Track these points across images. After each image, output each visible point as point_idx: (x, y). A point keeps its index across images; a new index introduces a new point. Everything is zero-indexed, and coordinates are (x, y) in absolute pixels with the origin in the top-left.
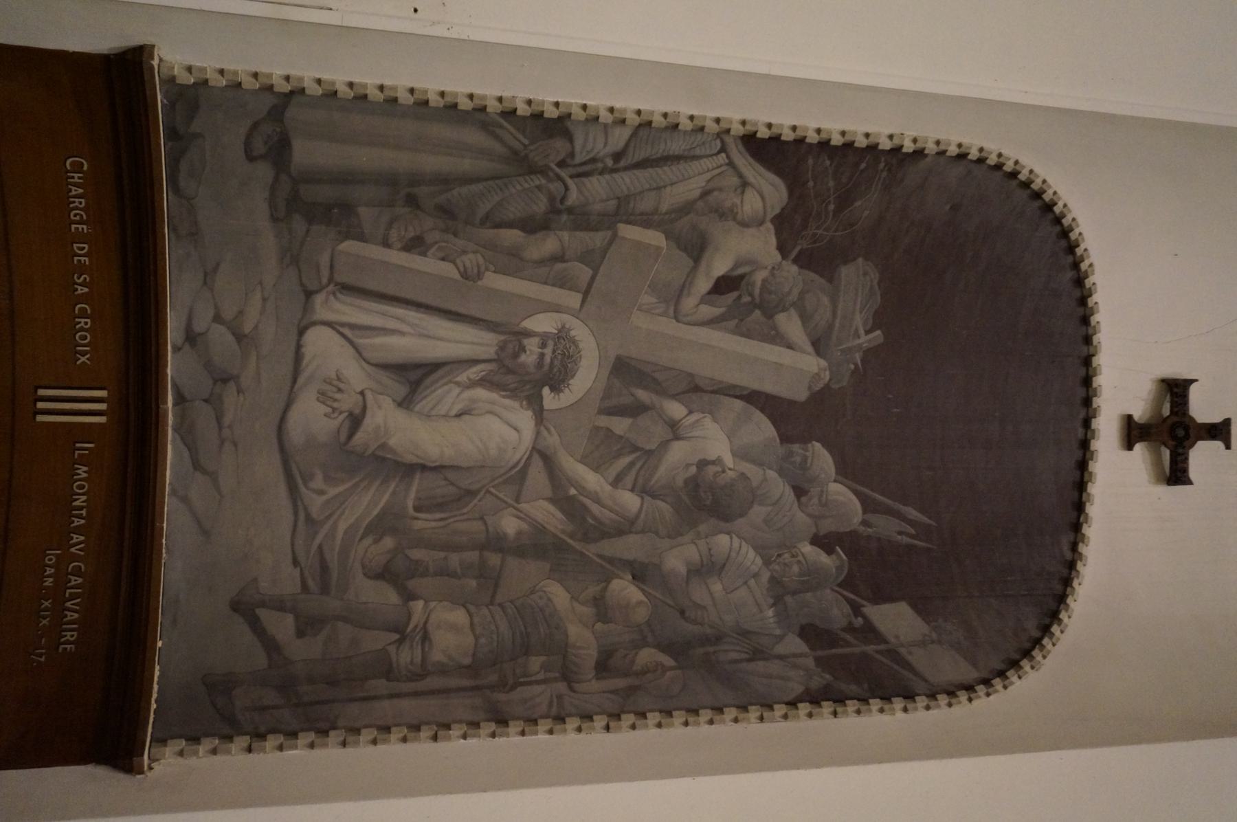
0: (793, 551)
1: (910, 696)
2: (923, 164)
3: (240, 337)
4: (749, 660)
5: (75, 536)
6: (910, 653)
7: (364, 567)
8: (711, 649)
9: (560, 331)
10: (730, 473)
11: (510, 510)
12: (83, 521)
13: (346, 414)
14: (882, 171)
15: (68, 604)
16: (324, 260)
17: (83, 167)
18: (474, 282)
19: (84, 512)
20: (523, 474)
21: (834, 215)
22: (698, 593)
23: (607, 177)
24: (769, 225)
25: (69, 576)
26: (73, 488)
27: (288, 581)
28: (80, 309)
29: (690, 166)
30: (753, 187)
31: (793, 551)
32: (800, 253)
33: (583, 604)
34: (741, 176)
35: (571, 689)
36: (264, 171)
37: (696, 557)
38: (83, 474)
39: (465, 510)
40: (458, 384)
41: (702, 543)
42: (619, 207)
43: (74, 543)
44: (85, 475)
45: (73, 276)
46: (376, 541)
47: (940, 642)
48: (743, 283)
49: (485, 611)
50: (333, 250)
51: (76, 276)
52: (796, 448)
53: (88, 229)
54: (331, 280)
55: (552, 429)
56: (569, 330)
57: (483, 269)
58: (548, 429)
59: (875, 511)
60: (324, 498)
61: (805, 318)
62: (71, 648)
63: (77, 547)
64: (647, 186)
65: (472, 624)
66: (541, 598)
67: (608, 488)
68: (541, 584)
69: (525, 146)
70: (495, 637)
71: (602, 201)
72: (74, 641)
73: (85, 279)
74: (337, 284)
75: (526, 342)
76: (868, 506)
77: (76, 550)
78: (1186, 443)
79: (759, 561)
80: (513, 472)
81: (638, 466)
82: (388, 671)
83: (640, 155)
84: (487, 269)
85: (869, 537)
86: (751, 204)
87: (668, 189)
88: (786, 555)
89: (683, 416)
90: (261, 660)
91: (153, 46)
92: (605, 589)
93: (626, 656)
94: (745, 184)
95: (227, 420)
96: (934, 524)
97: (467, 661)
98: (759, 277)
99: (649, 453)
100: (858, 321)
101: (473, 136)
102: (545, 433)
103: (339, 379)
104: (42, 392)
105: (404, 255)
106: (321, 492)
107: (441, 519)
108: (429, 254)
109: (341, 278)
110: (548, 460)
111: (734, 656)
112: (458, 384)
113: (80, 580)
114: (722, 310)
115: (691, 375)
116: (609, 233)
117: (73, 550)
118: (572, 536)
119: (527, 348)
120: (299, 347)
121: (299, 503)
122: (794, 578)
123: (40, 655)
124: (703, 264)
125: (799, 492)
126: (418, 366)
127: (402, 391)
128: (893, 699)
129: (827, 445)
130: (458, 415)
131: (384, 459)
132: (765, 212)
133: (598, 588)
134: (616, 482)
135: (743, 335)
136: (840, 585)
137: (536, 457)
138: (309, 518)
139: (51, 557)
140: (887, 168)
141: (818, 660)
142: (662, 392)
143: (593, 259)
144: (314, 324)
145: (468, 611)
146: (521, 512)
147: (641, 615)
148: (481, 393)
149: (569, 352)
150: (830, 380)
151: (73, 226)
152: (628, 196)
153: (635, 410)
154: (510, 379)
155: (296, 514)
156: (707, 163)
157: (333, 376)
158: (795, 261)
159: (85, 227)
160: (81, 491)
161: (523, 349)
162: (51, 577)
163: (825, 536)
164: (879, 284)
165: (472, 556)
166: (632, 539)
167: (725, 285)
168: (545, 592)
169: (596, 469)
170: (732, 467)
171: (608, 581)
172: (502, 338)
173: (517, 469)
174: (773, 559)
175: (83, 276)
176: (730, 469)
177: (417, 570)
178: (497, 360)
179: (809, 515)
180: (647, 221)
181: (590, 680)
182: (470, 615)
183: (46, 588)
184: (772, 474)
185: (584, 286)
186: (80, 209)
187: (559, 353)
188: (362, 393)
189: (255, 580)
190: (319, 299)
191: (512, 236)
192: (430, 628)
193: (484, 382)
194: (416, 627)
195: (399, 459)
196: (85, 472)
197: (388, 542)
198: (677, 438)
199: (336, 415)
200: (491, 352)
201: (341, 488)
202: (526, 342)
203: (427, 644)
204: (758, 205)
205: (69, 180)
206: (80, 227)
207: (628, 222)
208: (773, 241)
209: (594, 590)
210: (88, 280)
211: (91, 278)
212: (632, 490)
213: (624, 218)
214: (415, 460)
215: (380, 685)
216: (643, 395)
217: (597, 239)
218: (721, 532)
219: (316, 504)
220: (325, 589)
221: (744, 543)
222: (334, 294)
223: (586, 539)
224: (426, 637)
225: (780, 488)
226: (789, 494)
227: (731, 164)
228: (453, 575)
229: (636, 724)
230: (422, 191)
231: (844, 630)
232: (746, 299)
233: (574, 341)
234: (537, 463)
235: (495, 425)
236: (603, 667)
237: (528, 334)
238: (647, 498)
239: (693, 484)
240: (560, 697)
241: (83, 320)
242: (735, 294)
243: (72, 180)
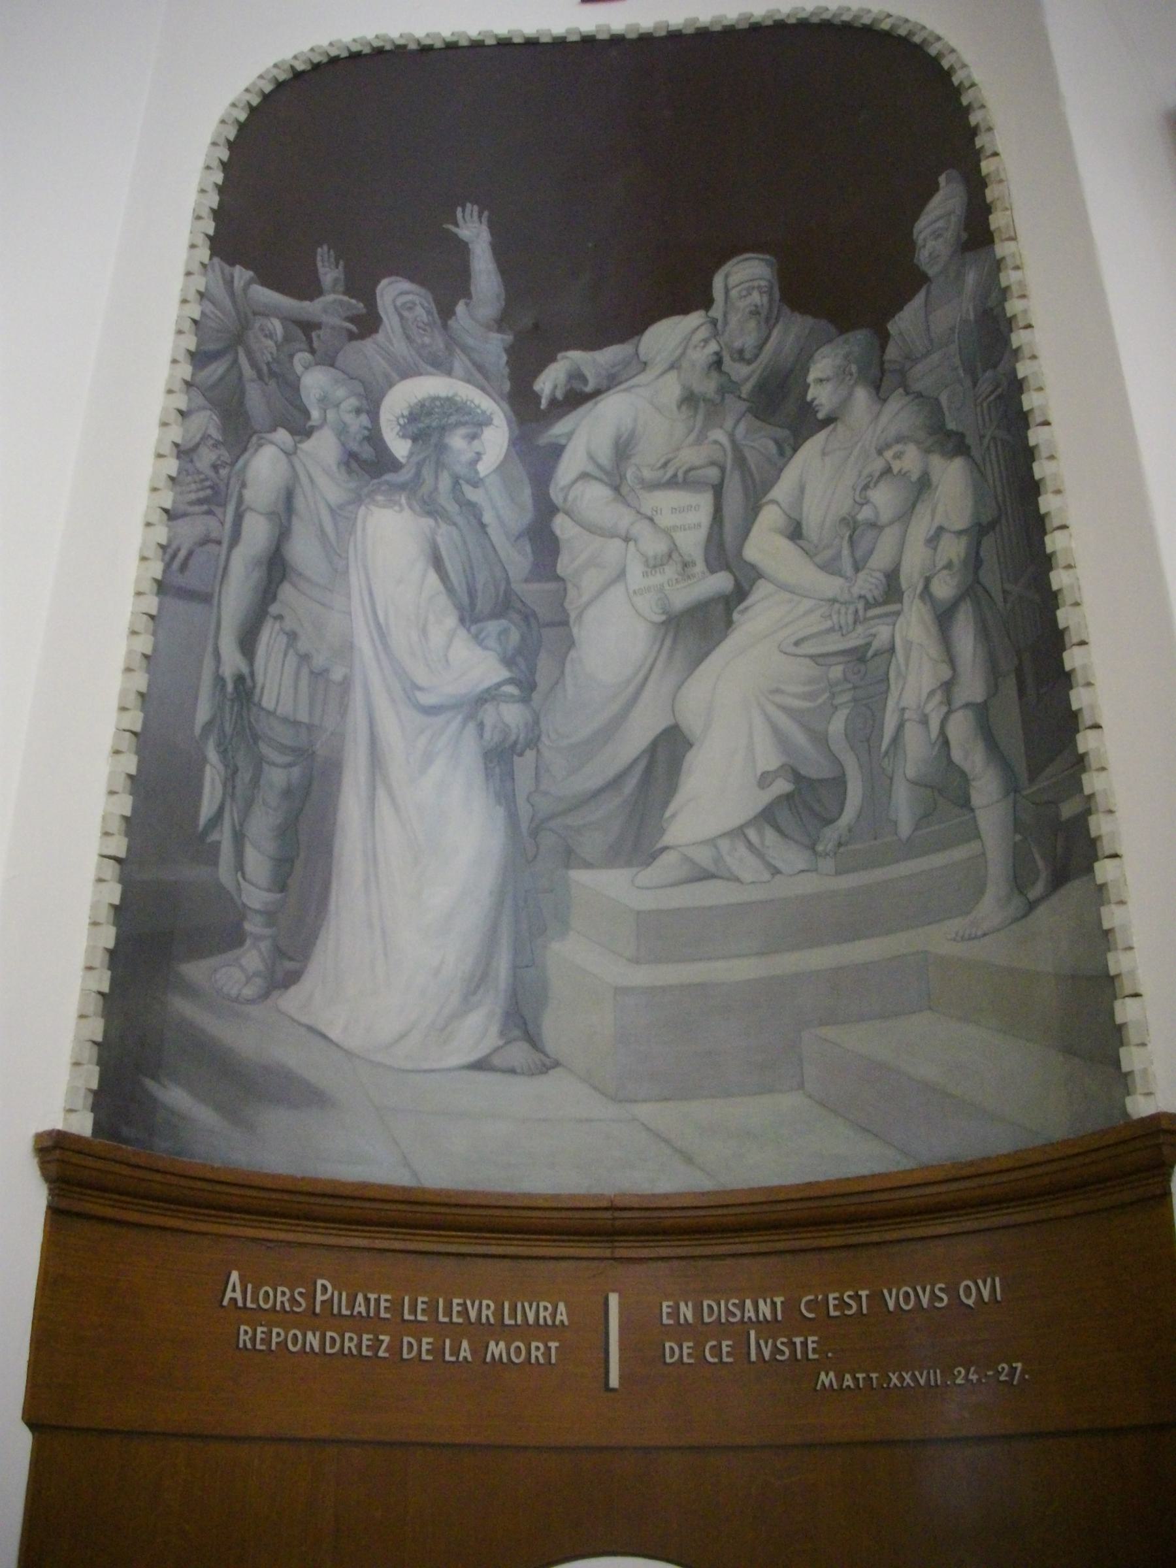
5: (229, 1294)
17: (812, 1300)
44: (502, 1345)
62: (668, 1307)
72: (357, 1335)
73: (782, 1343)
128: (1009, 315)
151: (425, 1357)
160: (715, 1308)
162: (757, 1302)
175: (847, 1300)
196: (497, 1345)
241: (242, 1337)
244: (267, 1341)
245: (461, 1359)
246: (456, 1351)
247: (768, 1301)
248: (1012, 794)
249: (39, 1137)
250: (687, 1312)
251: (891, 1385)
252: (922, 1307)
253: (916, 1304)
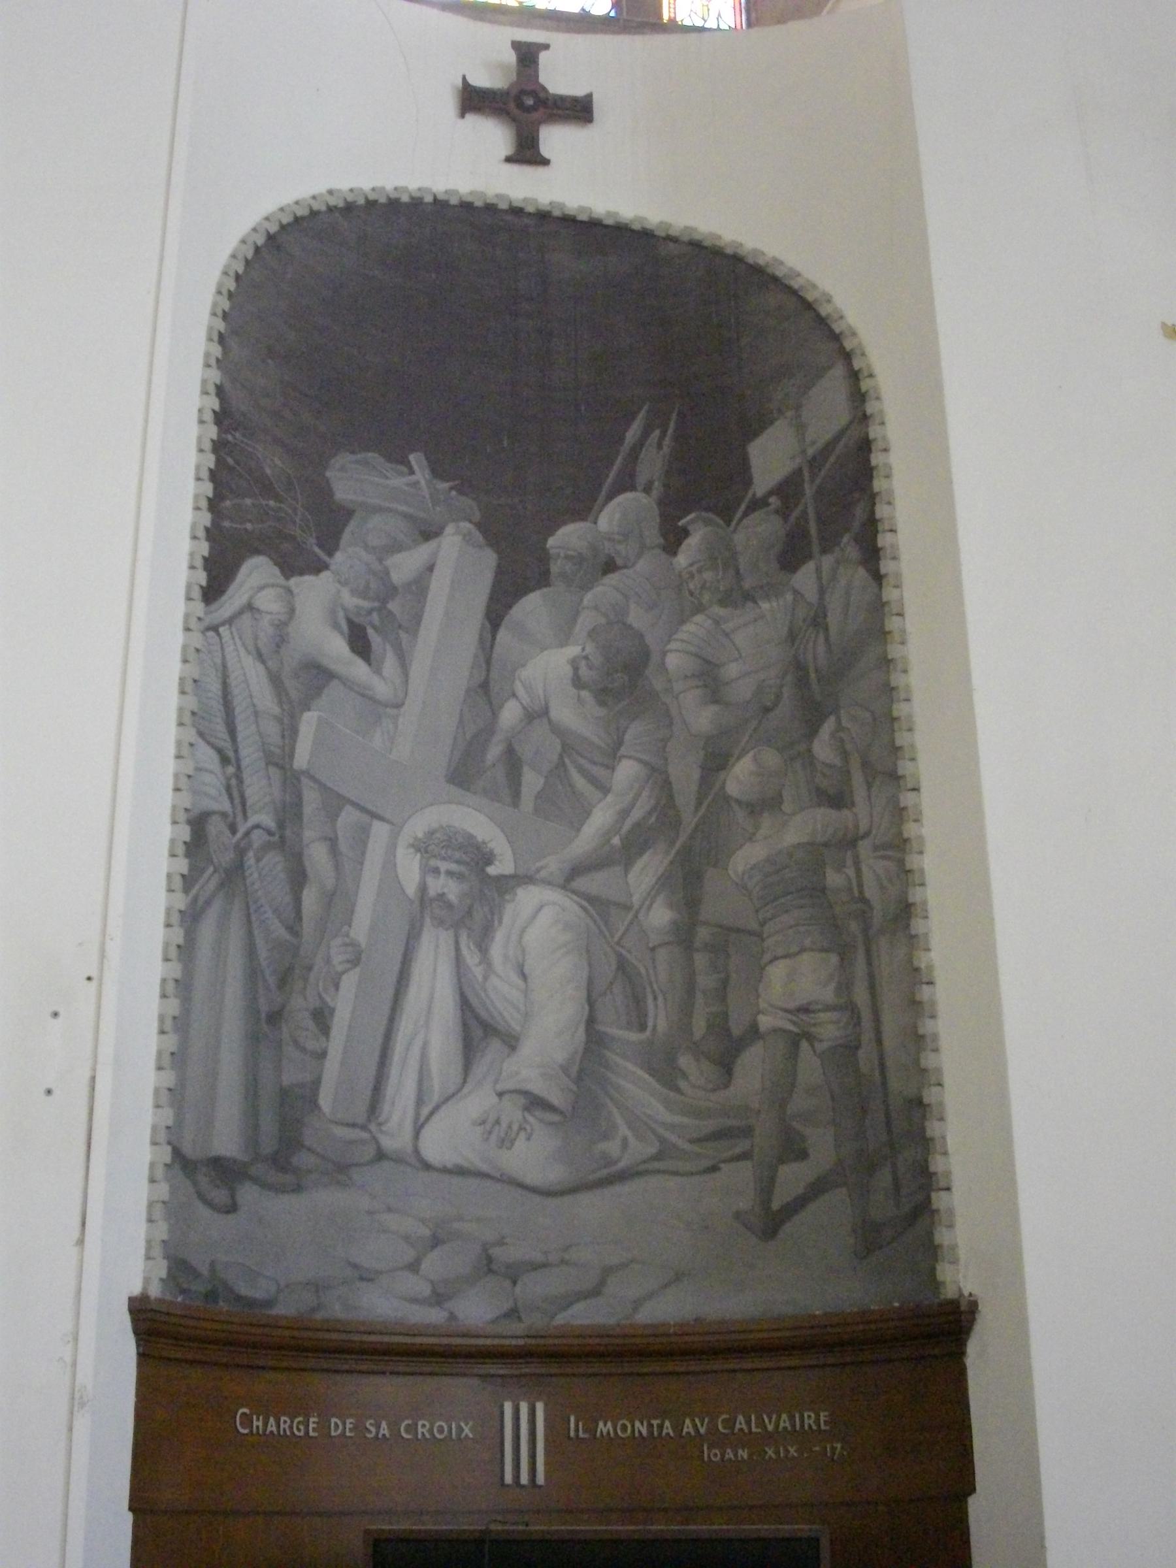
0: (685, 576)
1: (865, 446)
2: (228, 387)
3: (436, 1242)
4: (827, 629)
5: (685, 1430)
6: (813, 443)
7: (714, 1090)
8: (813, 676)
9: (418, 850)
10: (588, 650)
11: (641, 916)
12: (667, 1423)
13: (526, 1114)
14: (235, 438)
15: (770, 1428)
16: (340, 1132)
18: (362, 951)
19: (655, 1422)
20: (592, 900)
21: (281, 502)
22: (743, 691)
23: (245, 776)
24: (293, 582)
27: (742, 1176)
28: (407, 1431)
29: (233, 672)
30: (251, 598)
31: (685, 576)
32: (321, 546)
33: (757, 828)
34: (240, 612)
35: (867, 834)
36: (248, 1194)
37: (698, 692)
38: (607, 1427)
39: (643, 971)
40: (486, 978)
41: (678, 686)
42: (276, 765)
44: (609, 1424)
46: (684, 1075)
47: (798, 407)
48: (356, 620)
49: (769, 942)
50: (332, 1122)
52: (555, 568)
53: (314, 1416)
54: (364, 1128)
55: (538, 864)
56: (416, 838)
57: (347, 940)
58: (538, 870)
59: (632, 476)
60: (632, 1140)
61: (395, 547)
63: (699, 1425)
64: (253, 728)
65: (785, 957)
66: (750, 877)
67: (610, 798)
68: (733, 876)
69: (215, 871)
70: (802, 929)
71: (270, 785)
73: (371, 1424)
74: (369, 1120)
75: (432, 893)
76: (626, 483)
77: (702, 1425)
78: (542, 95)
79: (699, 618)
80: (593, 912)
81: (582, 761)
82: (850, 1048)
83: (221, 729)
84: (347, 935)
85: (666, 486)
86: (269, 602)
87: (255, 701)
88: (692, 586)
89: (518, 704)
90: (839, 1196)
91: (130, 1299)
92: (738, 802)
93: (824, 775)
94: (250, 607)
95: (538, 1257)
96: (646, 408)
97: (834, 959)
98: (350, 601)
99: (566, 748)
100: (399, 482)
101: (207, 931)
102: (543, 874)
103: (483, 1122)
104: (508, 1478)
105: (334, 1032)
106: (625, 1143)
107: (655, 998)
108: (331, 1004)
109: (359, 1111)
110: (576, 871)
111: (821, 648)
112: (486, 978)
113: (740, 1418)
114: (388, 647)
115: (468, 691)
116: (305, 781)
117: (702, 1431)
118: (672, 843)
119: (440, 891)
120: (445, 1170)
121: (642, 1167)
122: (719, 577)
123: (833, 1449)
124: (333, 667)
125: (610, 567)
126: (465, 1025)
127: (496, 1045)
129: (551, 531)
130: (524, 977)
131: (581, 1071)
132: (281, 587)
133: (736, 807)
134: (605, 790)
135: (419, 623)
136: (728, 523)
137: (574, 885)
138: (657, 1157)
139: (715, 1455)
140: (233, 432)
141: (824, 551)
142: (490, 729)
143: (334, 803)
144: (416, 1151)
145: (771, 962)
146: (643, 904)
147: (771, 758)
148: (496, 951)
149: (444, 841)
150: (471, 522)
152: (264, 751)
153: (513, 762)
154: (479, 915)
155: (646, 1172)
156: (229, 649)
157: (479, 1130)
158: (330, 554)
159: (312, 1420)
161: (442, 896)
162: (737, 1452)
163: (664, 535)
164: (353, 452)
165: (701, 960)
166: (675, 771)
167: (360, 644)
168: (743, 874)
169: (588, 814)
170: (580, 648)
171: (727, 799)
172: (428, 920)
173: (589, 908)
174: (696, 601)
175: (368, 1426)
176: (583, 649)
177: (719, 1025)
178: (457, 926)
179: (639, 556)
180: (291, 732)
181: (856, 815)
182: (776, 958)
183: (750, 1455)
184: (588, 598)
185: (366, 818)
186: (292, 1422)
187: (446, 853)
188: (500, 1095)
189: (737, 1215)
190: (387, 1143)
191: (310, 898)
192: (792, 1005)
193: (483, 949)
194: (794, 1023)
195: (581, 1050)
196: (605, 1425)
197: (685, 1061)
198: (545, 712)
199: (528, 1127)
200: (445, 937)
201: (619, 1121)
202: (432, 893)
203: (812, 1007)
204: (269, 593)
206: (311, 1426)
207: (292, 756)
208: (308, 578)
209: (740, 815)
210: (372, 1421)
211: (370, 1417)
212: (613, 769)
213: (287, 759)
214: (582, 1029)
215: (866, 1056)
216: (494, 751)
217: (311, 799)
218: (663, 663)
219: (640, 1150)
220: (747, 1132)
221: (675, 637)
222: (380, 1124)
223: (676, 824)
224: (805, 1010)
225: (606, 589)
226: (613, 579)
227: (230, 621)
228: (725, 983)
230: (264, 1007)
231: (785, 517)
232: (375, 617)
233: (431, 833)
234: (581, 883)
235: (533, 937)
236: (838, 800)
237: (423, 889)
238: (623, 751)
239: (603, 694)
240: (876, 848)
241: (420, 1430)
242: (370, 631)
243: (261, 1428)
244: (792, 1418)
250: (785, 1422)
251: (463, 1435)
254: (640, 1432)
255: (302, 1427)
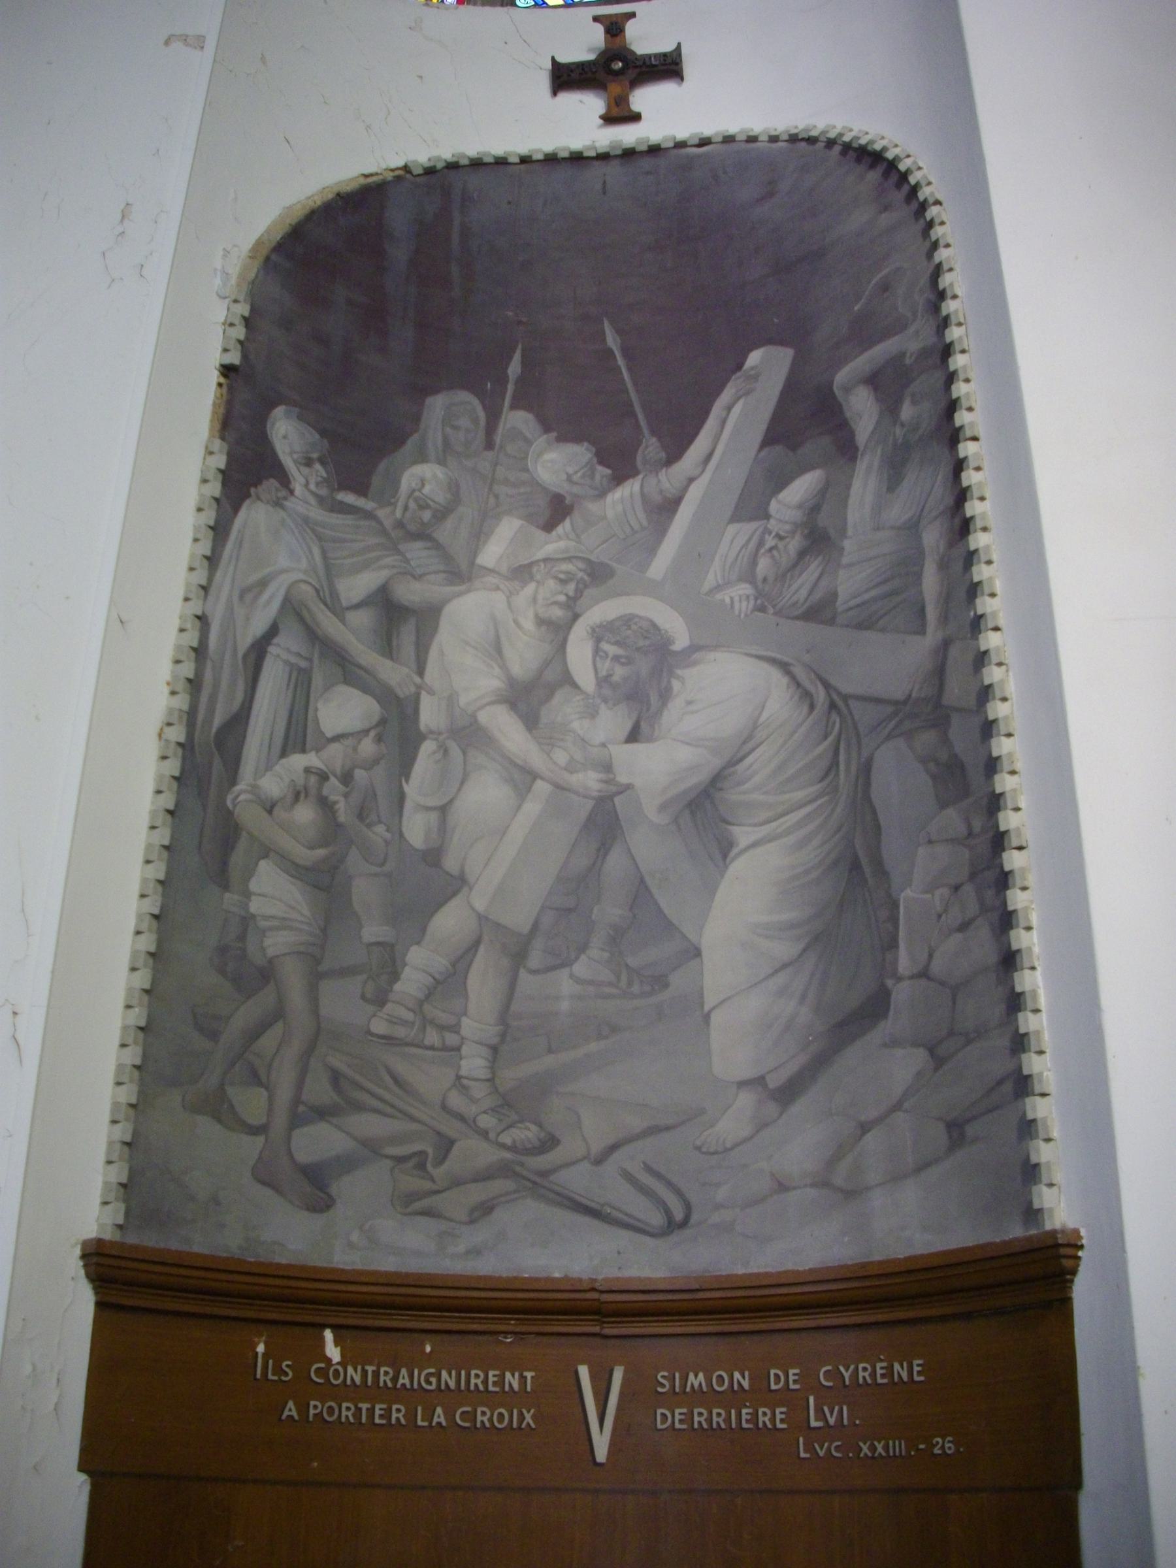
15: (832, 1421)
19: (364, 1406)
25: (434, 1424)
26: (722, 1392)
43: (520, 1384)
44: (701, 1375)
45: (285, 1382)
51: (660, 1389)
73: (663, 1377)
186: (492, 1415)
196: (696, 1376)
205: (677, 1390)
229: (1024, 926)
241: (479, 1418)
245: (393, 1421)
246: (430, 1415)
247: (359, 1368)
248: (945, 891)
249: (85, 1244)
252: (858, 1383)
253: (337, 1419)
254: (352, 1379)
255: (433, 1380)
